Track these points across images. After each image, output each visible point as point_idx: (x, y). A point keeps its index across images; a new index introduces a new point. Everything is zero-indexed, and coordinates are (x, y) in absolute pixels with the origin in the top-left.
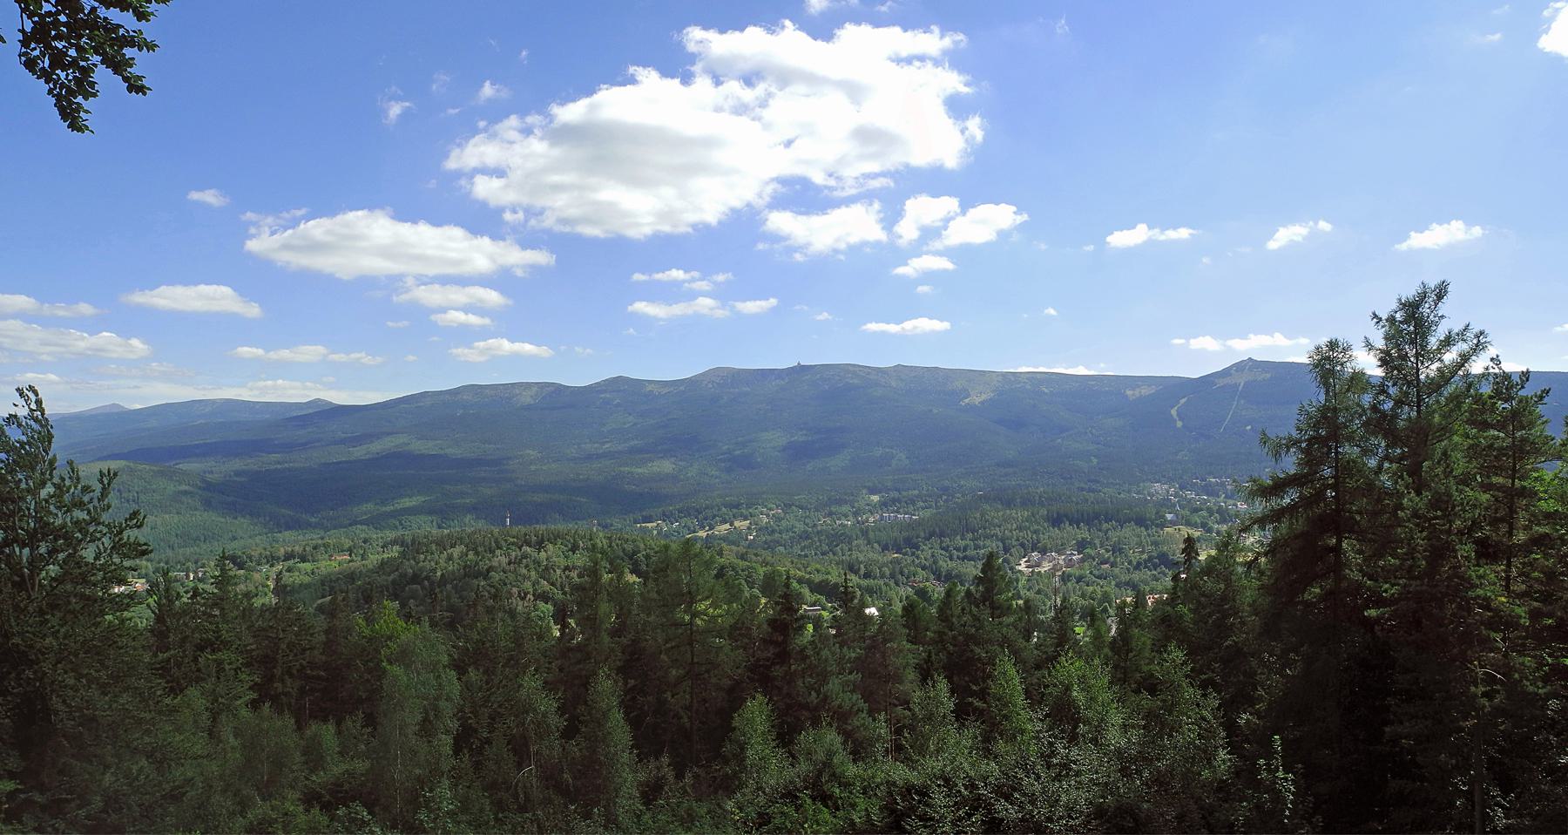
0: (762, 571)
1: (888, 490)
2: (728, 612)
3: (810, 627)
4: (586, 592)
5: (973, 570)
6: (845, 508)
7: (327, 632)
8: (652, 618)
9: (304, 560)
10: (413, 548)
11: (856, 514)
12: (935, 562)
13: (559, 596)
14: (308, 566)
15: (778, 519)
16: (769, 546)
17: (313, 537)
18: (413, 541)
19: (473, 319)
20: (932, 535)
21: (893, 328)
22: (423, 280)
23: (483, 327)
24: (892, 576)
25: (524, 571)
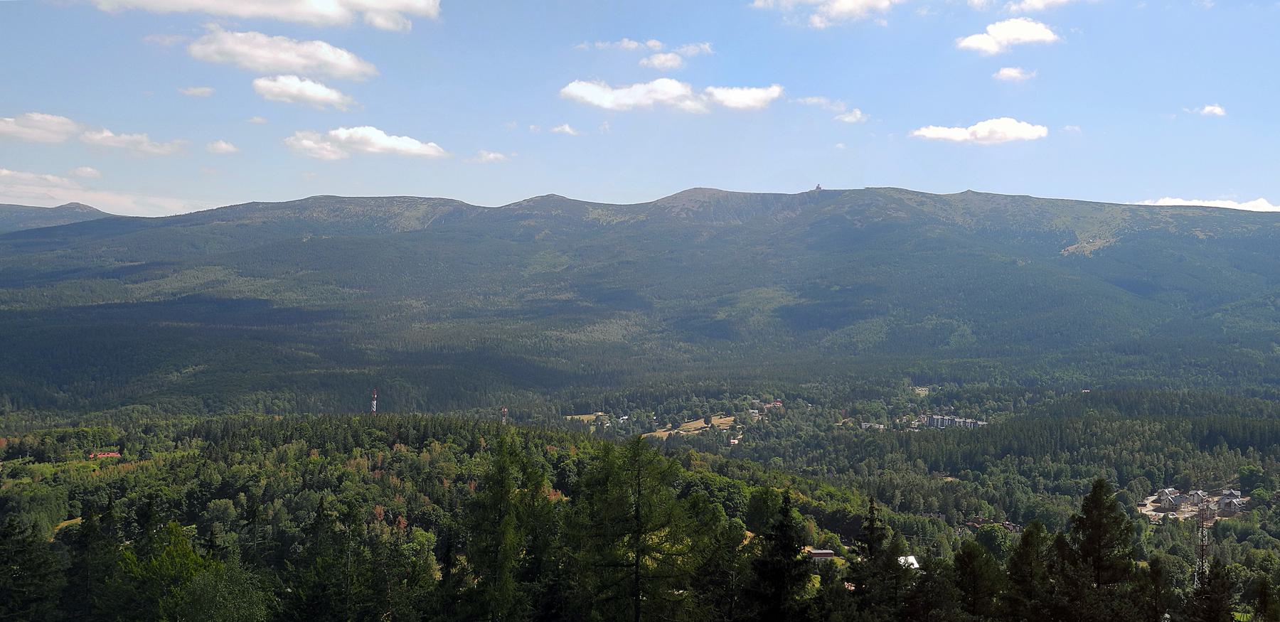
0: (748, 491)
1: (941, 380)
2: (692, 549)
3: (816, 580)
4: (488, 509)
5: (1068, 508)
6: (877, 405)
7: (69, 572)
8: (579, 555)
9: (40, 457)
10: (218, 441)
11: (892, 414)
12: (1010, 493)
13: (445, 519)
14: (47, 469)
15: (775, 416)
16: (762, 456)
17: (61, 423)
18: (225, 431)
19: (316, 91)
20: (1006, 451)
21: (958, 134)
22: (236, 24)
23: (328, 105)
24: (943, 510)
25: (395, 481)
